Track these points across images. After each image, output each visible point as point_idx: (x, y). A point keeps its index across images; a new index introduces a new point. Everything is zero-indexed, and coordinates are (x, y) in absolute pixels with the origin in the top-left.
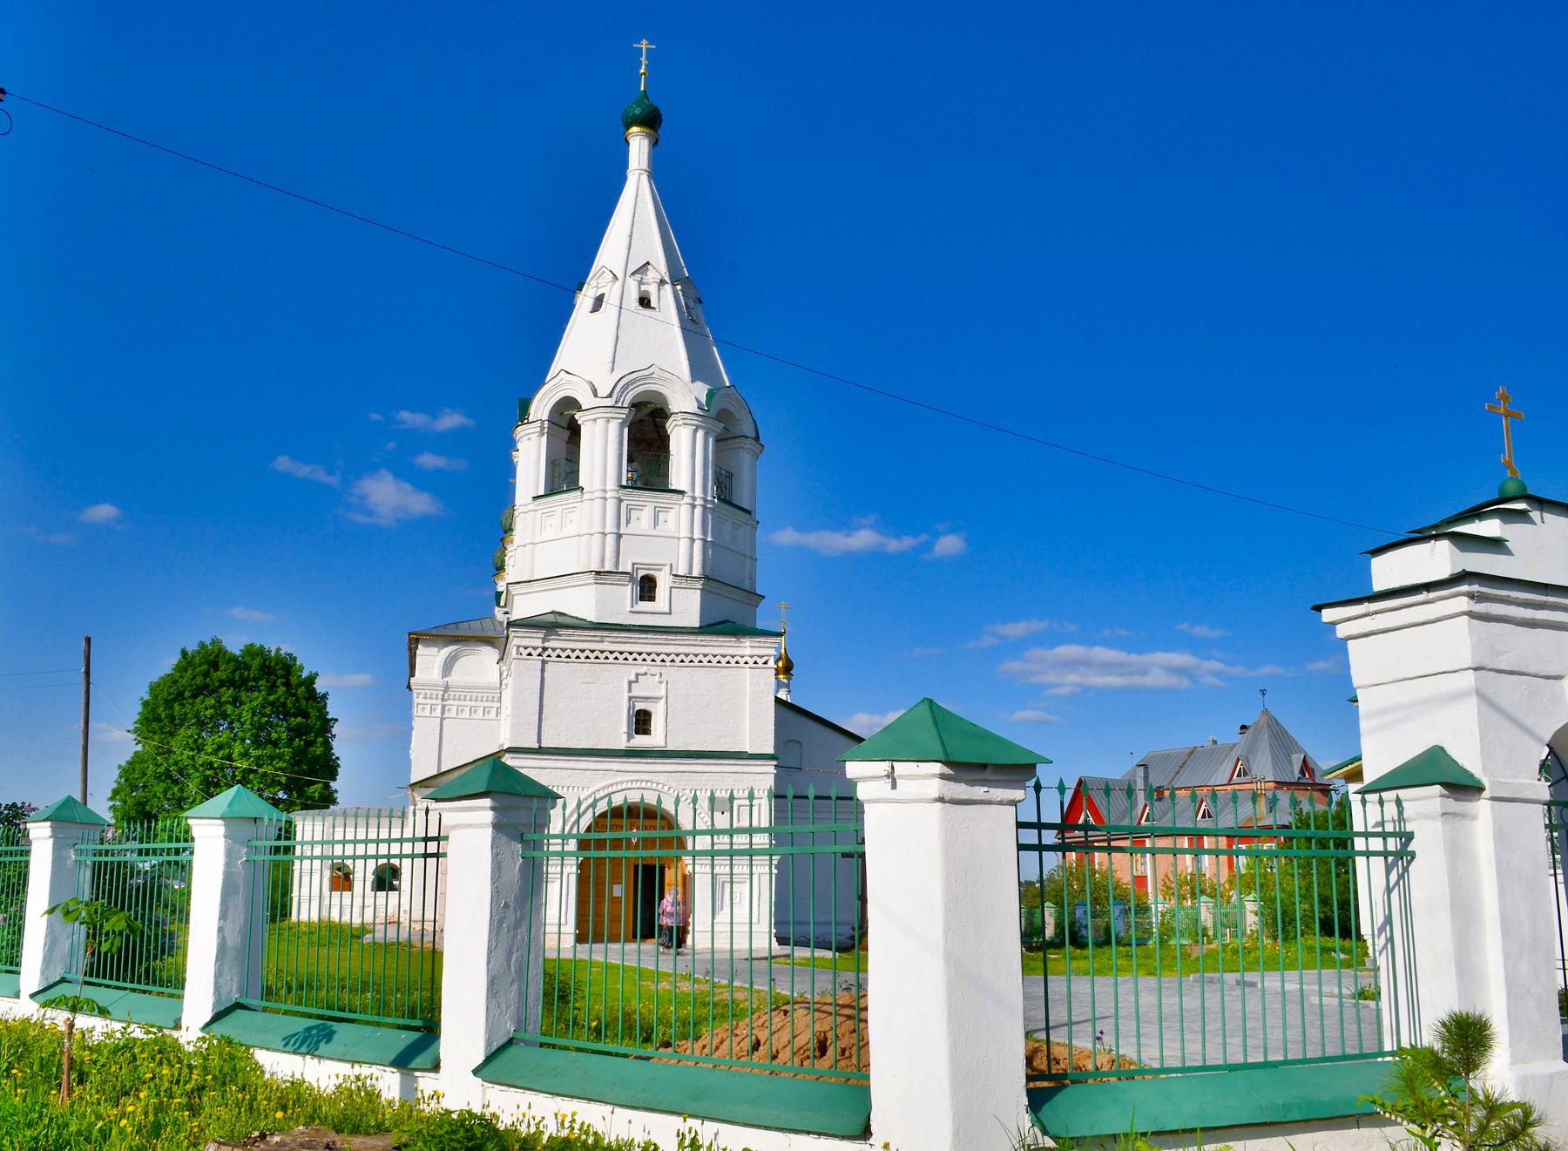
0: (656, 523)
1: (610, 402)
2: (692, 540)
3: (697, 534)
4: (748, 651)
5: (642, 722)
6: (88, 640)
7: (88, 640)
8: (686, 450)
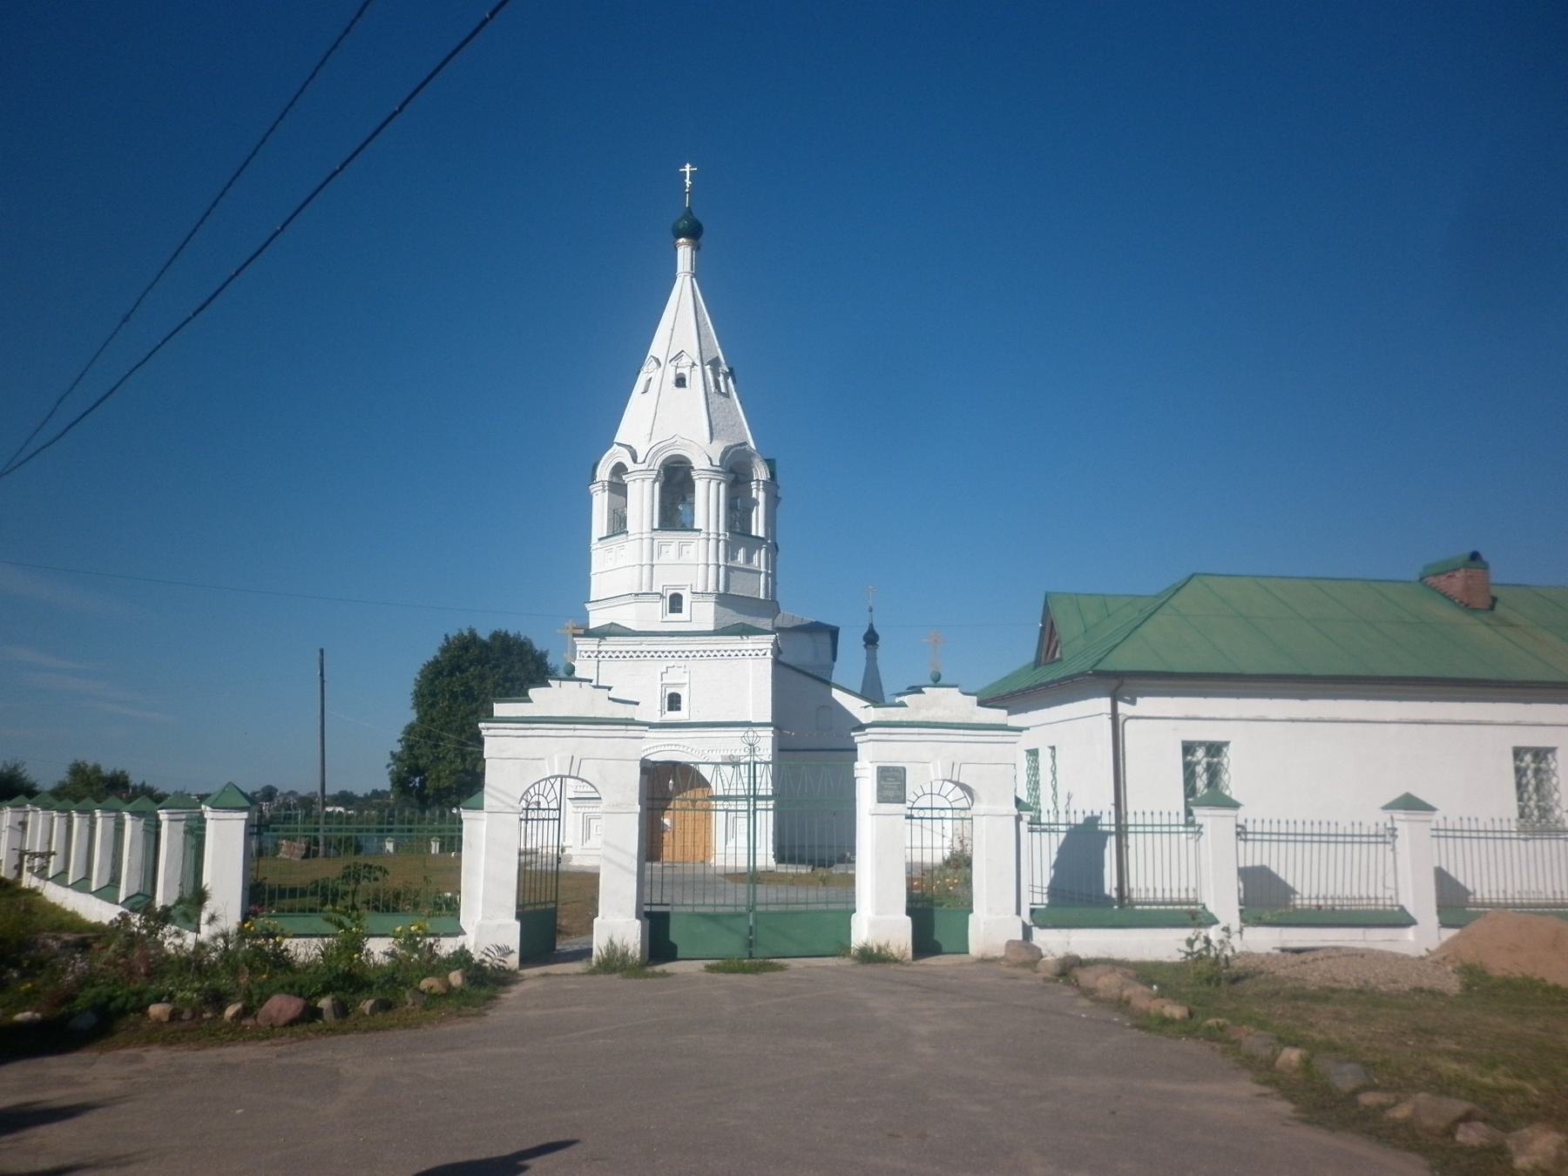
0: (680, 555)
1: (644, 467)
2: (718, 566)
3: (721, 562)
4: (751, 646)
5: (674, 702)
6: (322, 651)
7: (322, 651)
8: (707, 499)
